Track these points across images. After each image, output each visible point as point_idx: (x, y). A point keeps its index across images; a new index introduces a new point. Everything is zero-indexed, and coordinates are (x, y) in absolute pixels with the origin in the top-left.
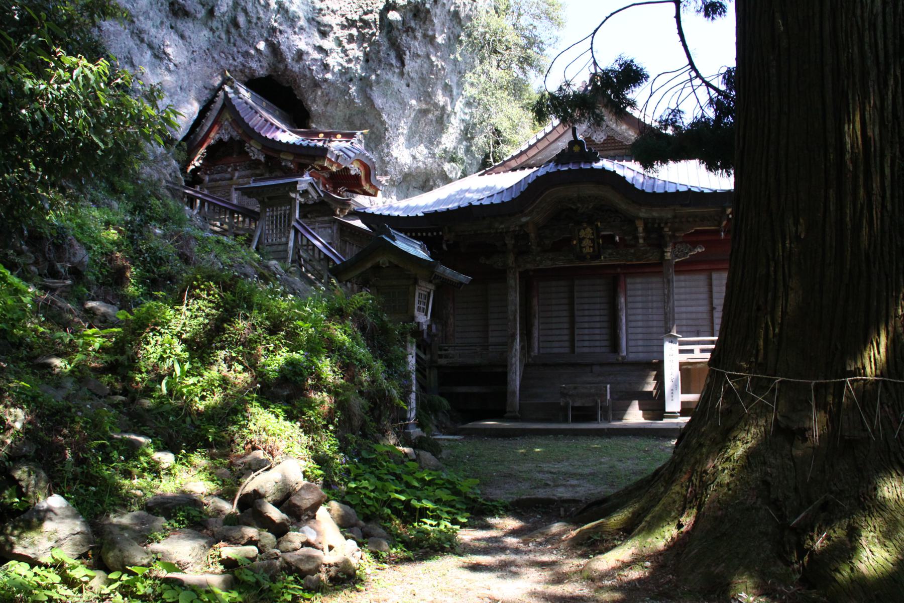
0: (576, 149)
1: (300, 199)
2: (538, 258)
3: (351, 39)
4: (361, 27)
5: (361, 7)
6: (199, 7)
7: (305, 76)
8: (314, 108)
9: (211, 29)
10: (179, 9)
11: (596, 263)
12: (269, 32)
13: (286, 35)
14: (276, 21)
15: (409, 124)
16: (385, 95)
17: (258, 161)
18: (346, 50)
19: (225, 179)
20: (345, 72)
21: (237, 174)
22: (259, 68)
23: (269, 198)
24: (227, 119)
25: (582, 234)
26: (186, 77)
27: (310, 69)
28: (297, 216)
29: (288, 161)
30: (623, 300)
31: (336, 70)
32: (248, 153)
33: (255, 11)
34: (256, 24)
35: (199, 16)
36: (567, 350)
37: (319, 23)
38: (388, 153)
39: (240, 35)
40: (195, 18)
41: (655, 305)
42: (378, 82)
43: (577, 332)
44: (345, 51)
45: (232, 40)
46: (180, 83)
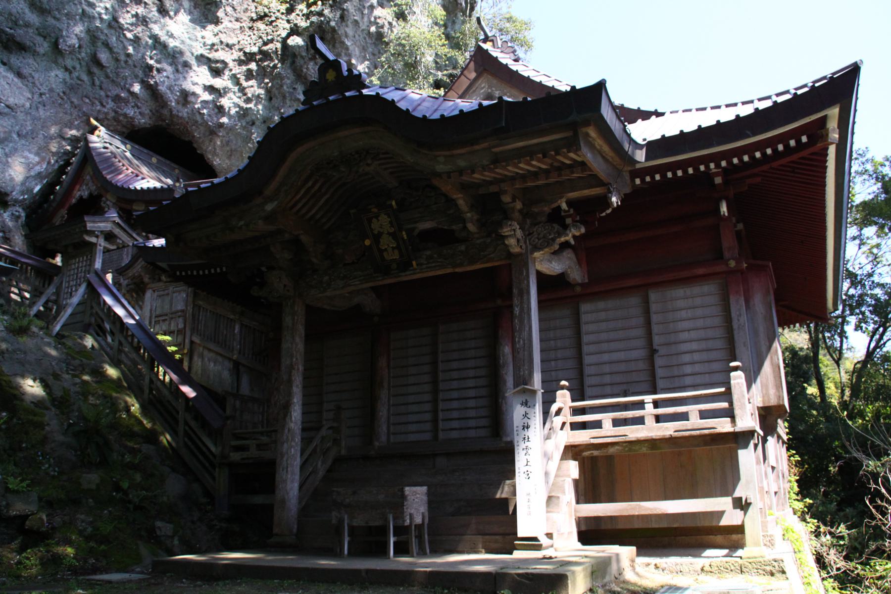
0: (331, 76)
2: (326, 278)
3: (249, 75)
4: (260, 60)
5: (261, 37)
6: (39, 39)
7: (197, 122)
9: (66, 69)
10: (8, 40)
11: (406, 277)
12: (144, 72)
13: (165, 74)
14: (151, 58)
18: (244, 88)
20: (244, 113)
22: (140, 115)
25: (375, 225)
27: (200, 113)
30: (507, 350)
31: (233, 111)
33: (121, 47)
34: (126, 62)
35: (41, 51)
36: (427, 436)
37: (209, 59)
39: (107, 77)
40: (35, 54)
41: (560, 354)
43: (441, 406)
44: (242, 90)
45: (97, 82)
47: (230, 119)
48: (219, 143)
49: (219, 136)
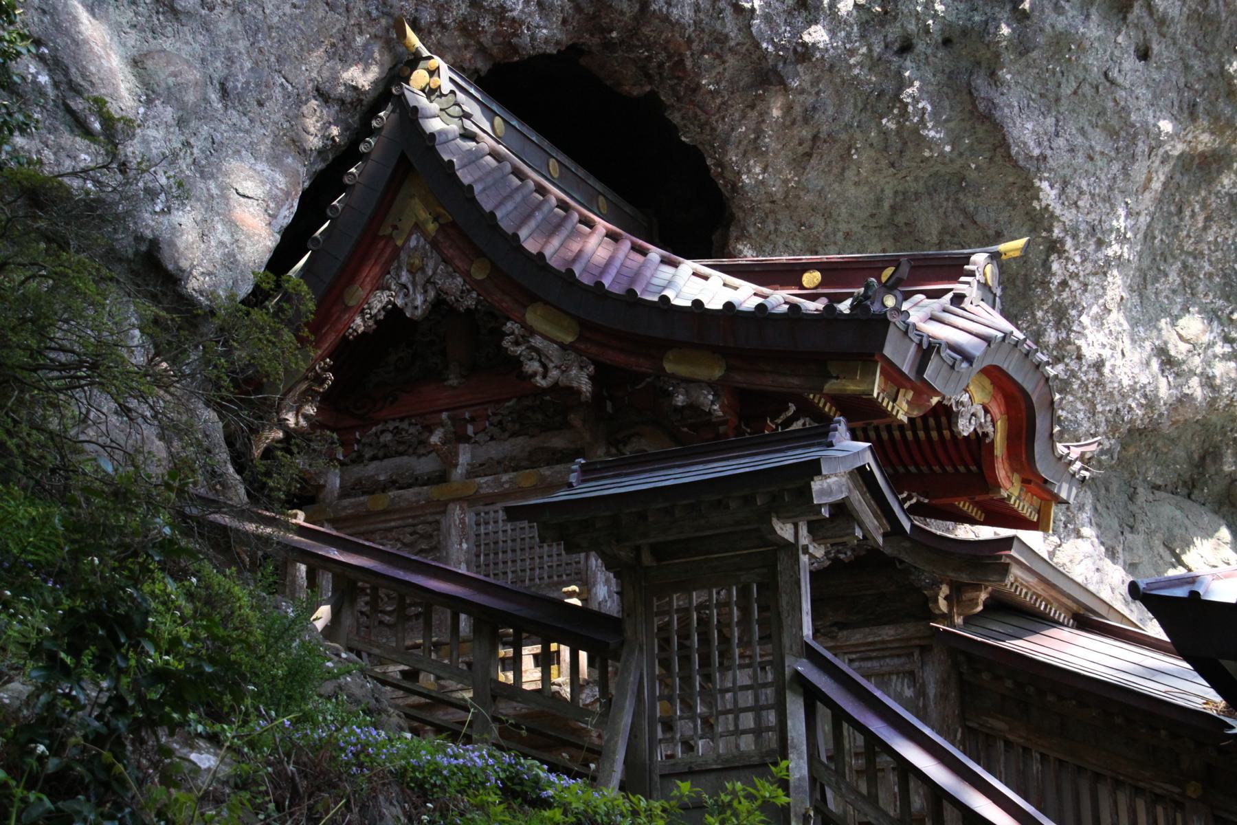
1: (812, 554)
7: (722, 39)
8: (752, 175)
15: (1144, 220)
16: (1049, 101)
17: (564, 392)
19: (416, 481)
21: (464, 457)
23: (659, 551)
24: (418, 227)
26: (242, 45)
28: (807, 630)
29: (699, 386)
32: (517, 362)
38: (1061, 345)
42: (1022, 46)
46: (218, 67)
47: (833, 33)
48: (776, 113)
49: (786, 89)
